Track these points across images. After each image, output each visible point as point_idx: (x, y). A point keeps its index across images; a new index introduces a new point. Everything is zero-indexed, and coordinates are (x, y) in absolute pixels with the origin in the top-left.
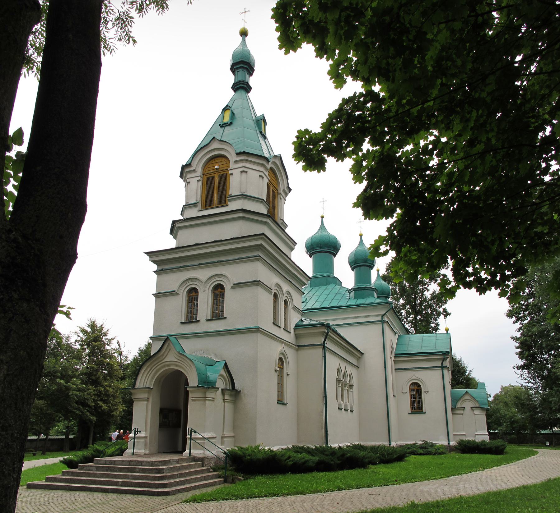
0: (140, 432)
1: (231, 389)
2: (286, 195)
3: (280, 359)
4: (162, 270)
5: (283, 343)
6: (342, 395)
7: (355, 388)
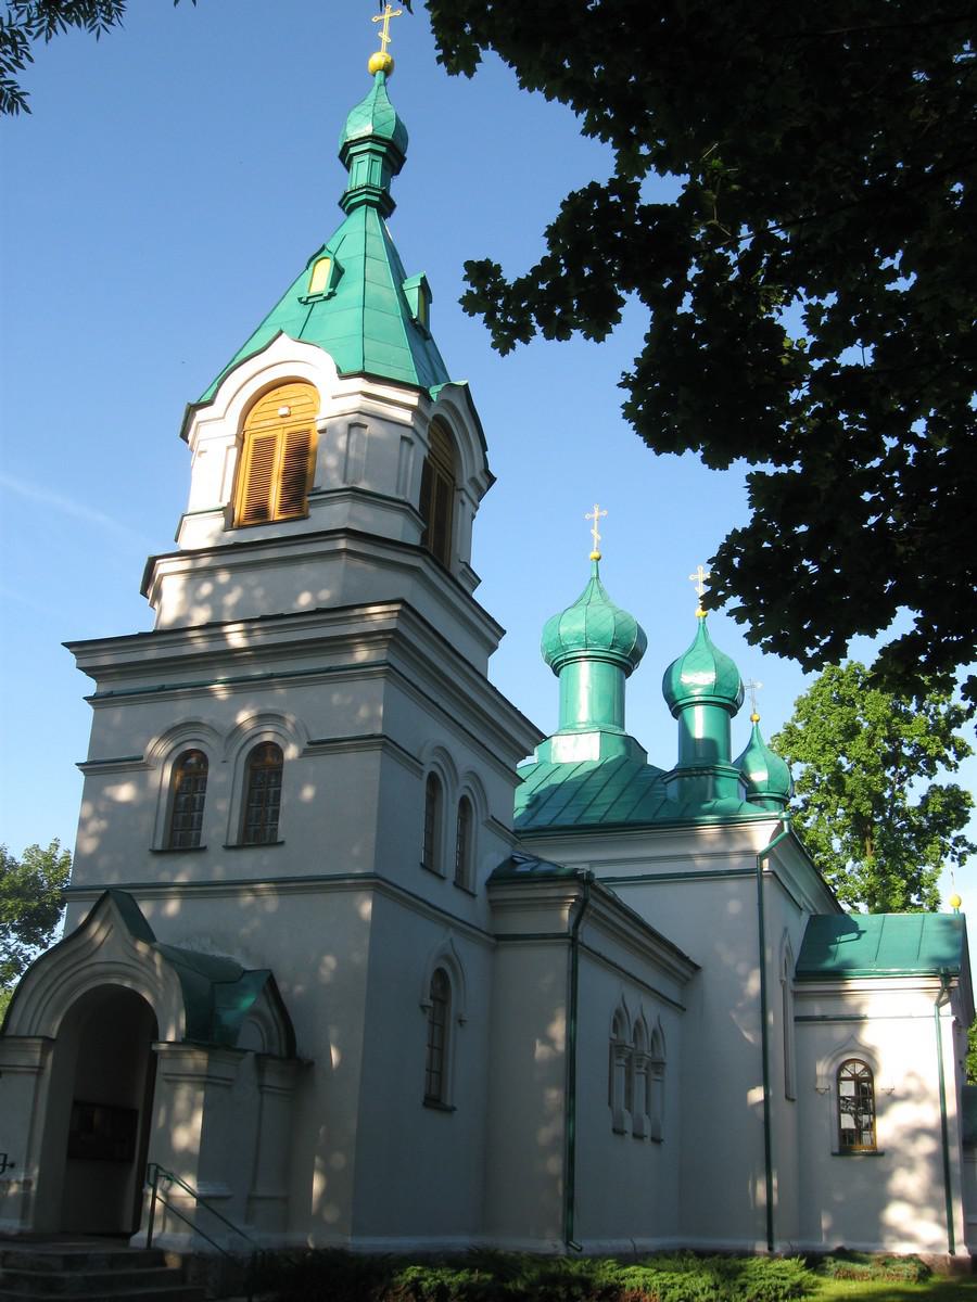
0: (12, 1166)
1: (284, 1053)
2: (481, 493)
3: (440, 974)
4: (110, 695)
5: (450, 925)
6: (629, 1092)
7: (671, 1071)
